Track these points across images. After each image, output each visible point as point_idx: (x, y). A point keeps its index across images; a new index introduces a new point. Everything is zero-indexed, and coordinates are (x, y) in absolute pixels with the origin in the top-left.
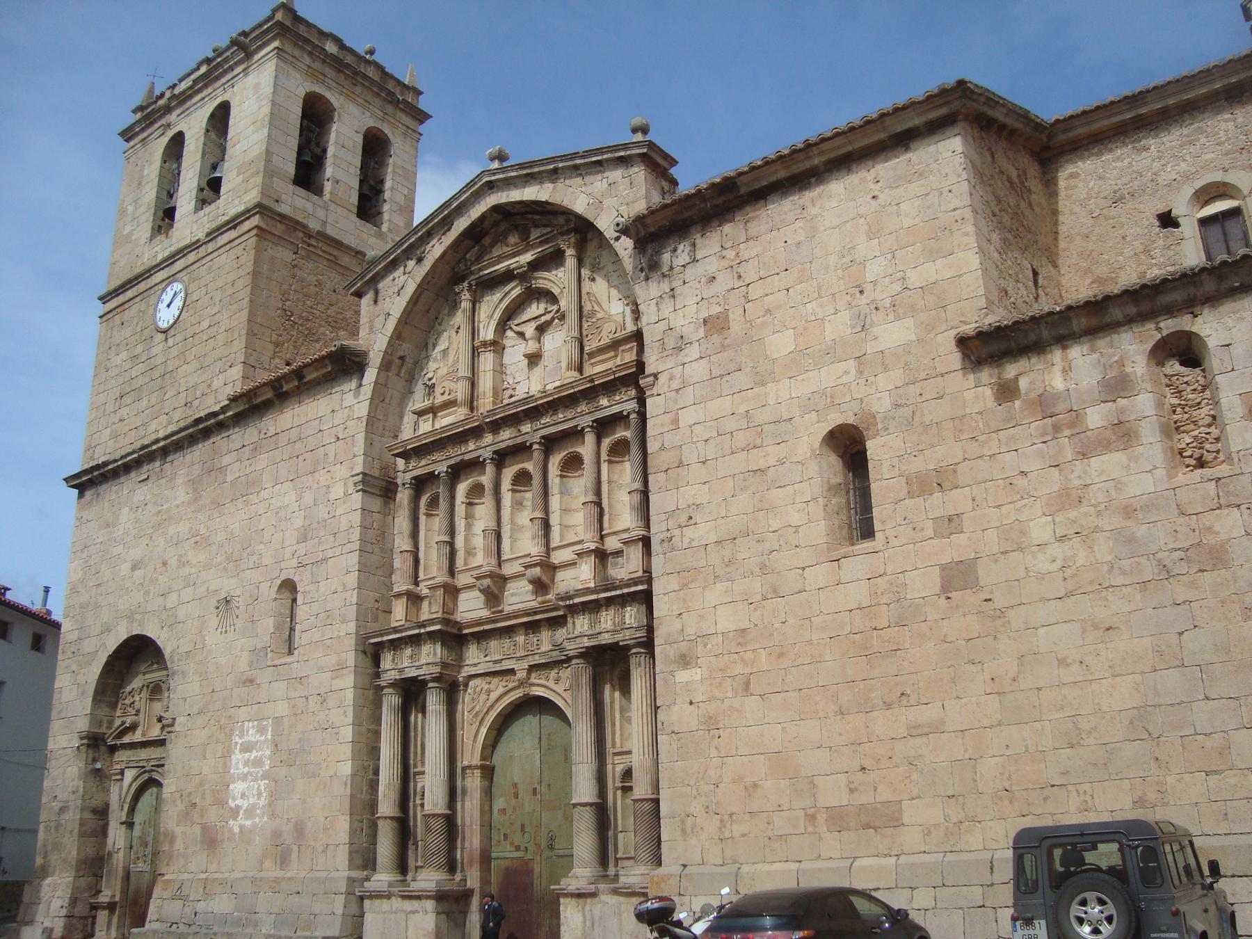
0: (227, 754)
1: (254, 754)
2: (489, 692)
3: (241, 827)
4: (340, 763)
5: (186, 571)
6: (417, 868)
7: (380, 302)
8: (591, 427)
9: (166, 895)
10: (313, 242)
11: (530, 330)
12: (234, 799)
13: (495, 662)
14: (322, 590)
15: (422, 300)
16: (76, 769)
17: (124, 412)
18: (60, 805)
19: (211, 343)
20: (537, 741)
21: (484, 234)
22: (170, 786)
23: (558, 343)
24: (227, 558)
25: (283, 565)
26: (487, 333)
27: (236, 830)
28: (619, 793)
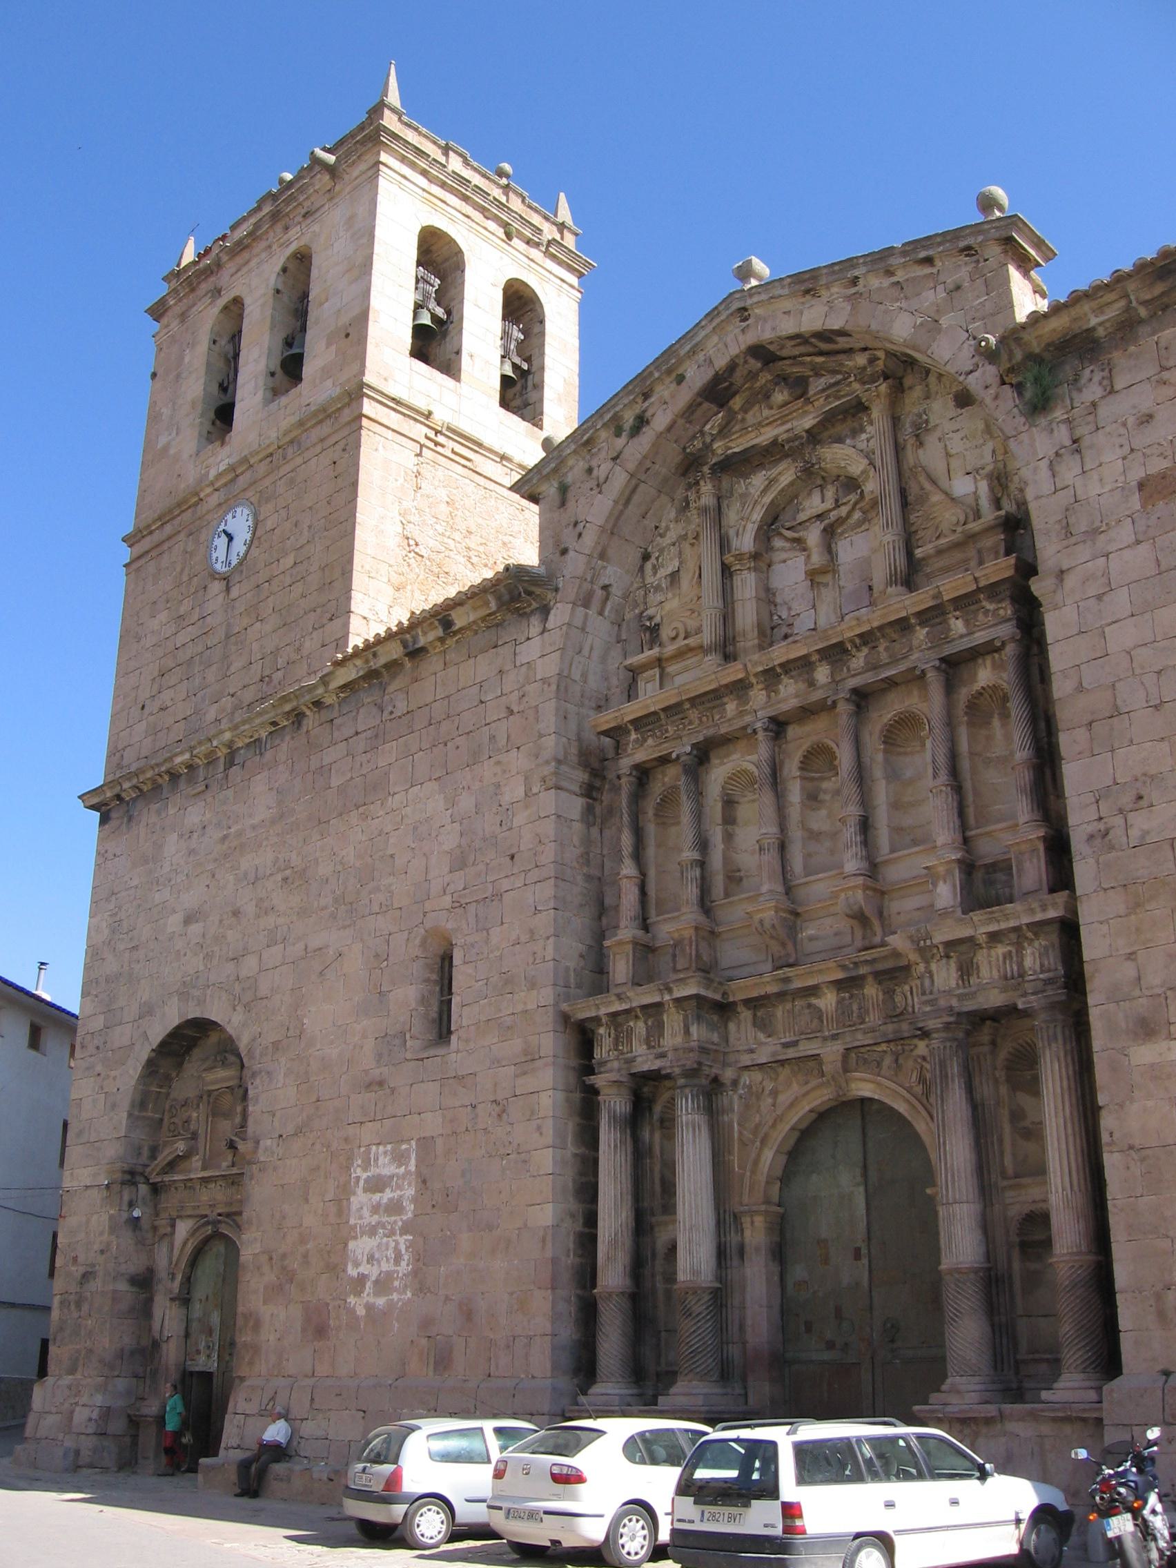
0: (345, 1191)
1: (388, 1195)
2: (775, 1093)
3: (369, 1307)
4: (543, 1210)
5: (270, 921)
6: (658, 1375)
7: (571, 504)
8: (938, 669)
9: (252, 1408)
10: (440, 439)
11: (813, 536)
12: (357, 1264)
13: (786, 1045)
14: (494, 940)
15: (636, 498)
16: (105, 1217)
17: (166, 696)
18: (82, 1270)
19: (298, 589)
20: (858, 1171)
21: (729, 393)
22: (251, 1246)
23: (868, 548)
24: (336, 900)
25: (428, 906)
26: (745, 542)
27: (361, 1311)
28: (1016, 1253)
